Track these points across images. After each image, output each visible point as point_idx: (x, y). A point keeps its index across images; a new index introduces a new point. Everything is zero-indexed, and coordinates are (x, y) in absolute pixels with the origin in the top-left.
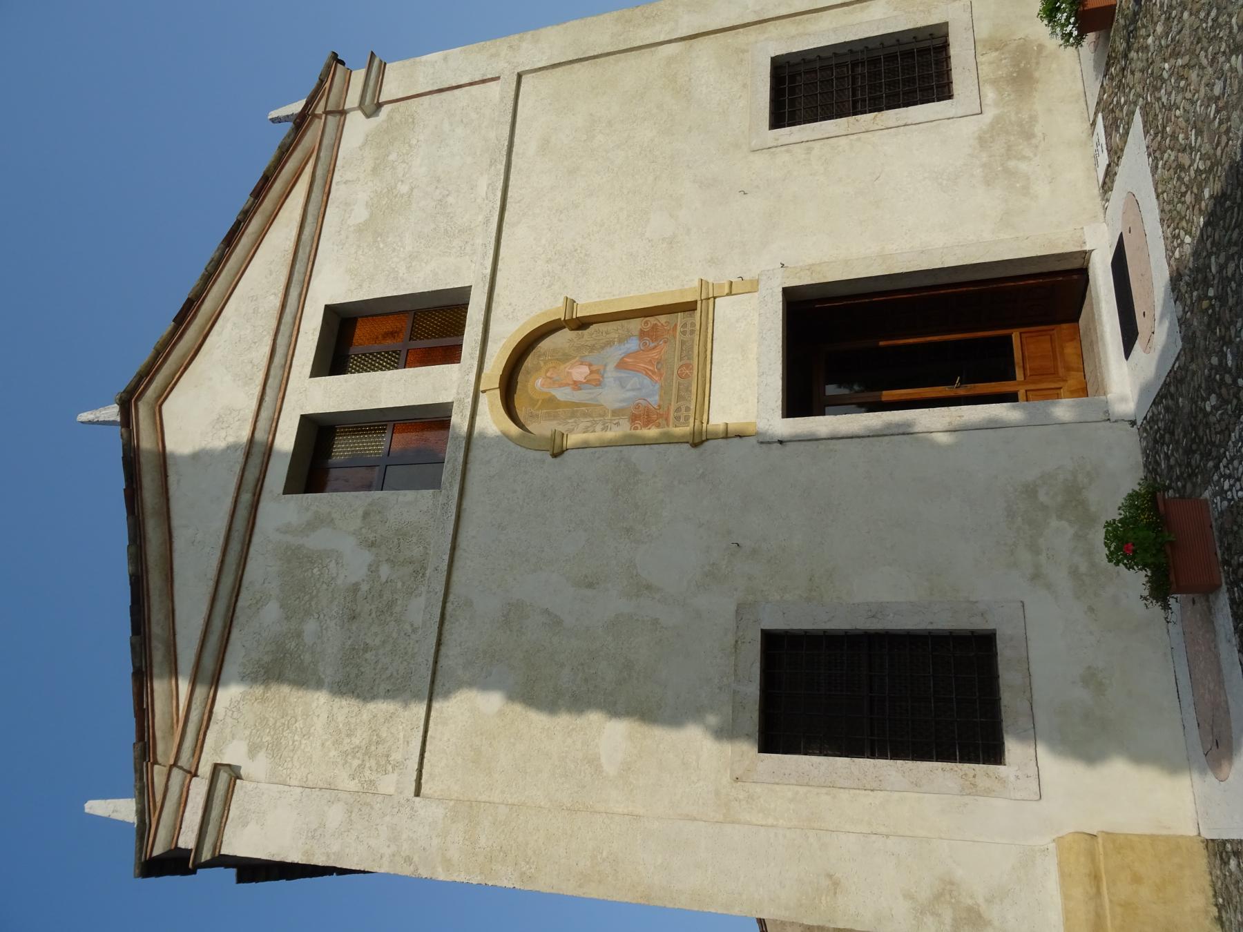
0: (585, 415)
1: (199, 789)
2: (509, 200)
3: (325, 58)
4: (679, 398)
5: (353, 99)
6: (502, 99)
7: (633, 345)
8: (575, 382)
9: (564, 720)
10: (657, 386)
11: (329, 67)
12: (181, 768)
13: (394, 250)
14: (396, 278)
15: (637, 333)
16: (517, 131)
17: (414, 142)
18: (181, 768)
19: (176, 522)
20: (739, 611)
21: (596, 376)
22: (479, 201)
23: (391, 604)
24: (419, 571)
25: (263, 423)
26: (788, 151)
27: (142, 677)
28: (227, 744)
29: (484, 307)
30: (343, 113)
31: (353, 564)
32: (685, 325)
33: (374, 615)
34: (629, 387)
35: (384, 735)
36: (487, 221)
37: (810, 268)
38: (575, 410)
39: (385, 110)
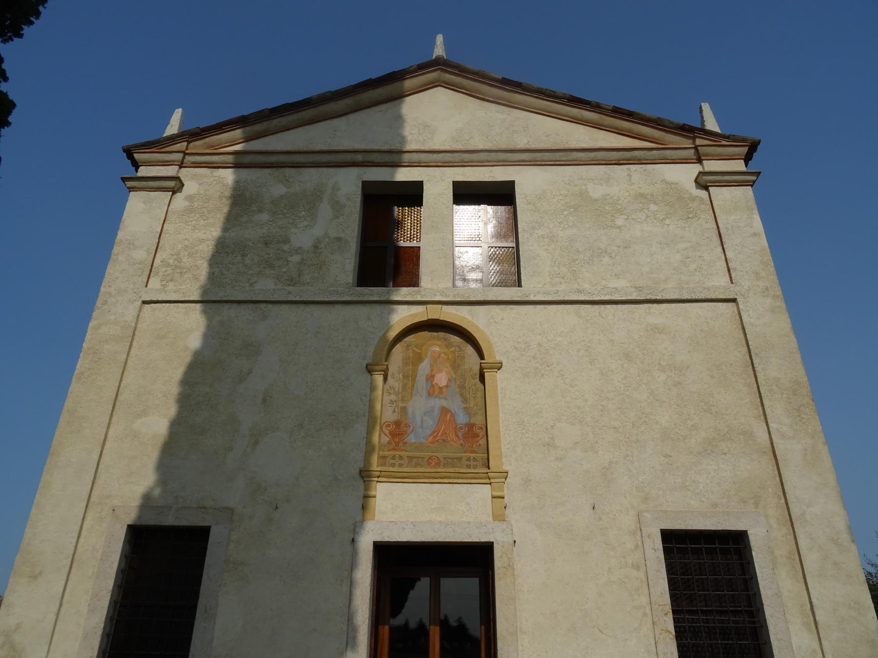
0: (404, 386)
1: (171, 171)
2: (602, 306)
3: (753, 135)
4: (411, 458)
5: (711, 166)
6: (708, 289)
7: (462, 419)
8: (433, 376)
9: (174, 390)
10: (423, 440)
11: (744, 140)
12: (184, 158)
13: (561, 223)
14: (534, 228)
15: (472, 421)
16: (673, 305)
17: (667, 222)
18: (184, 158)
19: (352, 117)
20: (230, 511)
21: (437, 391)
22: (604, 283)
23: (272, 266)
24: (292, 282)
25: (415, 157)
26: (637, 546)
27: (241, 122)
28: (195, 181)
29: (500, 299)
30: (700, 161)
31: (302, 237)
32: (475, 459)
33: (266, 256)
34: (425, 418)
35: (185, 276)
36: (579, 291)
37: (510, 566)
38: (409, 378)
39: (703, 194)
